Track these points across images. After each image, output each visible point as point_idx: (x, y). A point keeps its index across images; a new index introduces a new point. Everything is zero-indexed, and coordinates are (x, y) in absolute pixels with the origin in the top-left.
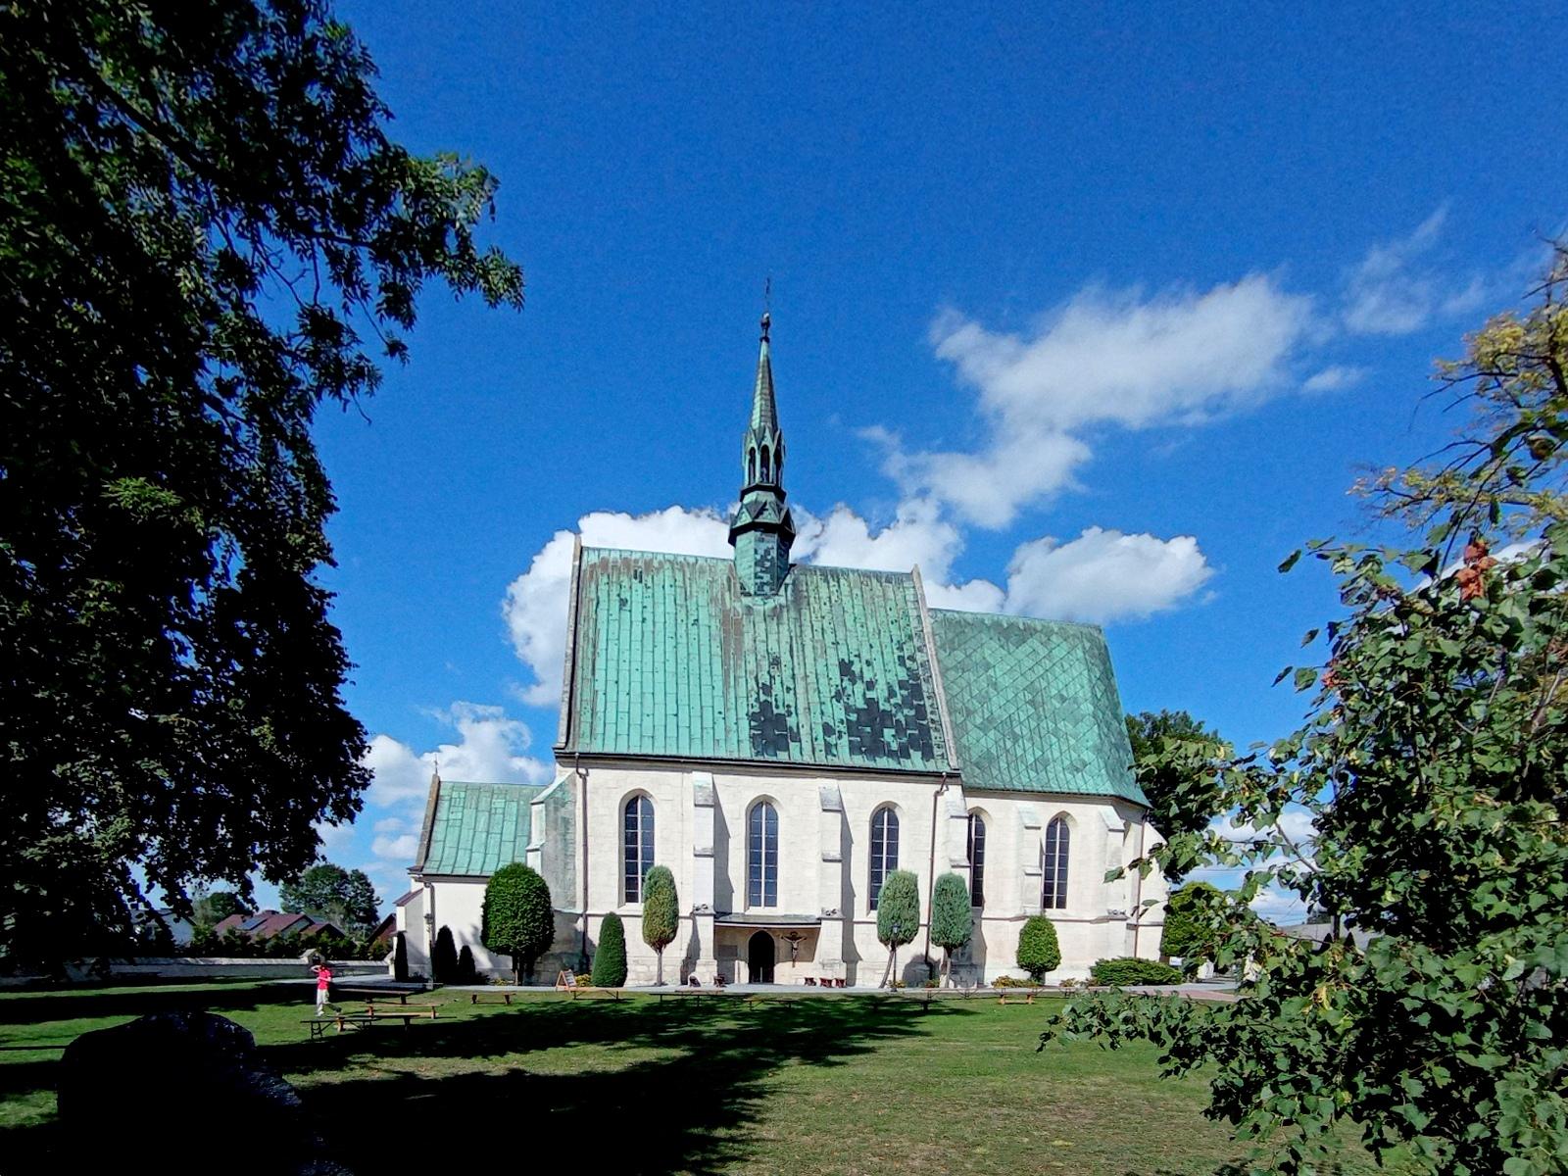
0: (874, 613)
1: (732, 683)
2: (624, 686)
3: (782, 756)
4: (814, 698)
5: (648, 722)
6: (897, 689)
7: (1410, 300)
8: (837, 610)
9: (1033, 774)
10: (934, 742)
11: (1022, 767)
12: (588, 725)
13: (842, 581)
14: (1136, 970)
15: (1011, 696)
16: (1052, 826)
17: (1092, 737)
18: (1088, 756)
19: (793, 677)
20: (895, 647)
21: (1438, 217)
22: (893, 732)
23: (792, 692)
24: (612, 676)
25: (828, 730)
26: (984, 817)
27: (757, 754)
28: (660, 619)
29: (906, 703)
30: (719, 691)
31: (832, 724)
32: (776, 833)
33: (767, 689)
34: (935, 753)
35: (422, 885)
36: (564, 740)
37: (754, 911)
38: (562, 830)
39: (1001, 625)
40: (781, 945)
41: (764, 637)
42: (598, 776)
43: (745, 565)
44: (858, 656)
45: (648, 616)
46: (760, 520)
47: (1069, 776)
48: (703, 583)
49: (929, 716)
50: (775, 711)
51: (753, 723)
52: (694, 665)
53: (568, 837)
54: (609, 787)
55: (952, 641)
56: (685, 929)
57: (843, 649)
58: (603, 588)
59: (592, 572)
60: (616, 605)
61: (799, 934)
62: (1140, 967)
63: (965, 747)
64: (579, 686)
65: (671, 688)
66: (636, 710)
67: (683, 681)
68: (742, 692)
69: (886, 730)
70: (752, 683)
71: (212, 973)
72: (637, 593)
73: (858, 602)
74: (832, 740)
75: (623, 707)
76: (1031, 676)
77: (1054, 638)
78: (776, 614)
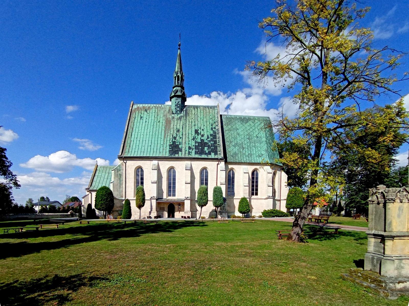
0: (206, 117)
1: (166, 137)
2: (138, 139)
3: (177, 156)
4: (187, 140)
5: (143, 148)
6: (209, 136)
7: (387, 30)
8: (196, 116)
9: (247, 158)
10: (218, 150)
11: (244, 156)
12: (128, 149)
13: (198, 109)
14: (273, 213)
15: (243, 137)
16: (253, 173)
17: (265, 147)
18: (263, 152)
19: (182, 134)
20: (210, 125)
21: (394, 9)
22: (207, 148)
23: (181, 138)
24: (136, 137)
25: (190, 148)
26: (234, 170)
27: (170, 155)
28: (150, 121)
29: (212, 140)
30: (162, 139)
31: (191, 146)
32: (175, 176)
33: (175, 138)
34: (218, 153)
35: (89, 193)
36: (121, 153)
37: (169, 198)
38: (119, 177)
39: (242, 118)
40: (176, 207)
41: (176, 124)
42: (129, 163)
43: (173, 106)
44: (200, 128)
45: (147, 121)
46: (177, 94)
47: (258, 158)
48: (162, 111)
49: (218, 143)
50: (176, 144)
51: (170, 147)
52: (157, 133)
53: (121, 179)
54: (132, 165)
55: (228, 123)
56: (147, 204)
57: (196, 126)
58: (137, 114)
59: (135, 110)
60: (139, 118)
61: (181, 204)
62: (274, 212)
63: (229, 151)
64: (127, 140)
65: (150, 139)
66: (140, 146)
67: (154, 137)
68: (168, 139)
69: (205, 148)
70: (171, 137)
71: (43, 217)
72: (145, 115)
73: (202, 114)
74: (190, 151)
75: (137, 144)
76: (249, 131)
77: (256, 121)
78: (180, 118)
